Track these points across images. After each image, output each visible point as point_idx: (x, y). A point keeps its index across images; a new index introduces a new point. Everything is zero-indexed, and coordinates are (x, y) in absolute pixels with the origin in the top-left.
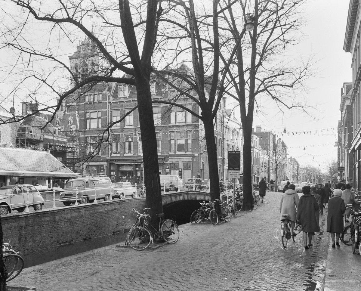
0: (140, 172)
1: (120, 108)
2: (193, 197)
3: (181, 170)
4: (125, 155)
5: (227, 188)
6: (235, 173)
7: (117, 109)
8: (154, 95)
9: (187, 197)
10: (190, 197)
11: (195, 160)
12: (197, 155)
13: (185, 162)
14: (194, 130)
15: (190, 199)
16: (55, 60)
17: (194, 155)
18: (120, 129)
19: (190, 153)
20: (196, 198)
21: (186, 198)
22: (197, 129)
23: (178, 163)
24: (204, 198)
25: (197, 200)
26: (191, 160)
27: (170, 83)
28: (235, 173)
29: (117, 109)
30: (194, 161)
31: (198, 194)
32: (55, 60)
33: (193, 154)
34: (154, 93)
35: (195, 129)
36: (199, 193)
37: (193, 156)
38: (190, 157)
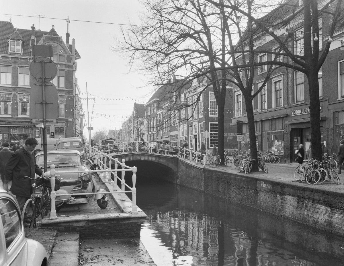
0: (2, 135)
1: (12, 65)
2: (138, 158)
3: (54, 134)
4: (19, 116)
5: (166, 150)
6: (240, 137)
7: (7, 65)
8: (20, 54)
9: (133, 158)
10: (135, 158)
11: (69, 125)
12: (71, 120)
13: (58, 126)
14: (68, 95)
15: (135, 160)
16: (214, 35)
17: (67, 120)
18: (11, 87)
19: (64, 118)
20: (140, 159)
21: (131, 159)
22: (71, 95)
23: (50, 127)
24: (148, 158)
25: (141, 160)
26: (64, 124)
27: (203, 62)
28: (240, 137)
29: (7, 65)
30: (68, 126)
31: (142, 155)
32: (214, 35)
33: (67, 118)
34: (21, 52)
35: (69, 95)
36: (143, 154)
37: (67, 121)
38: (63, 121)
